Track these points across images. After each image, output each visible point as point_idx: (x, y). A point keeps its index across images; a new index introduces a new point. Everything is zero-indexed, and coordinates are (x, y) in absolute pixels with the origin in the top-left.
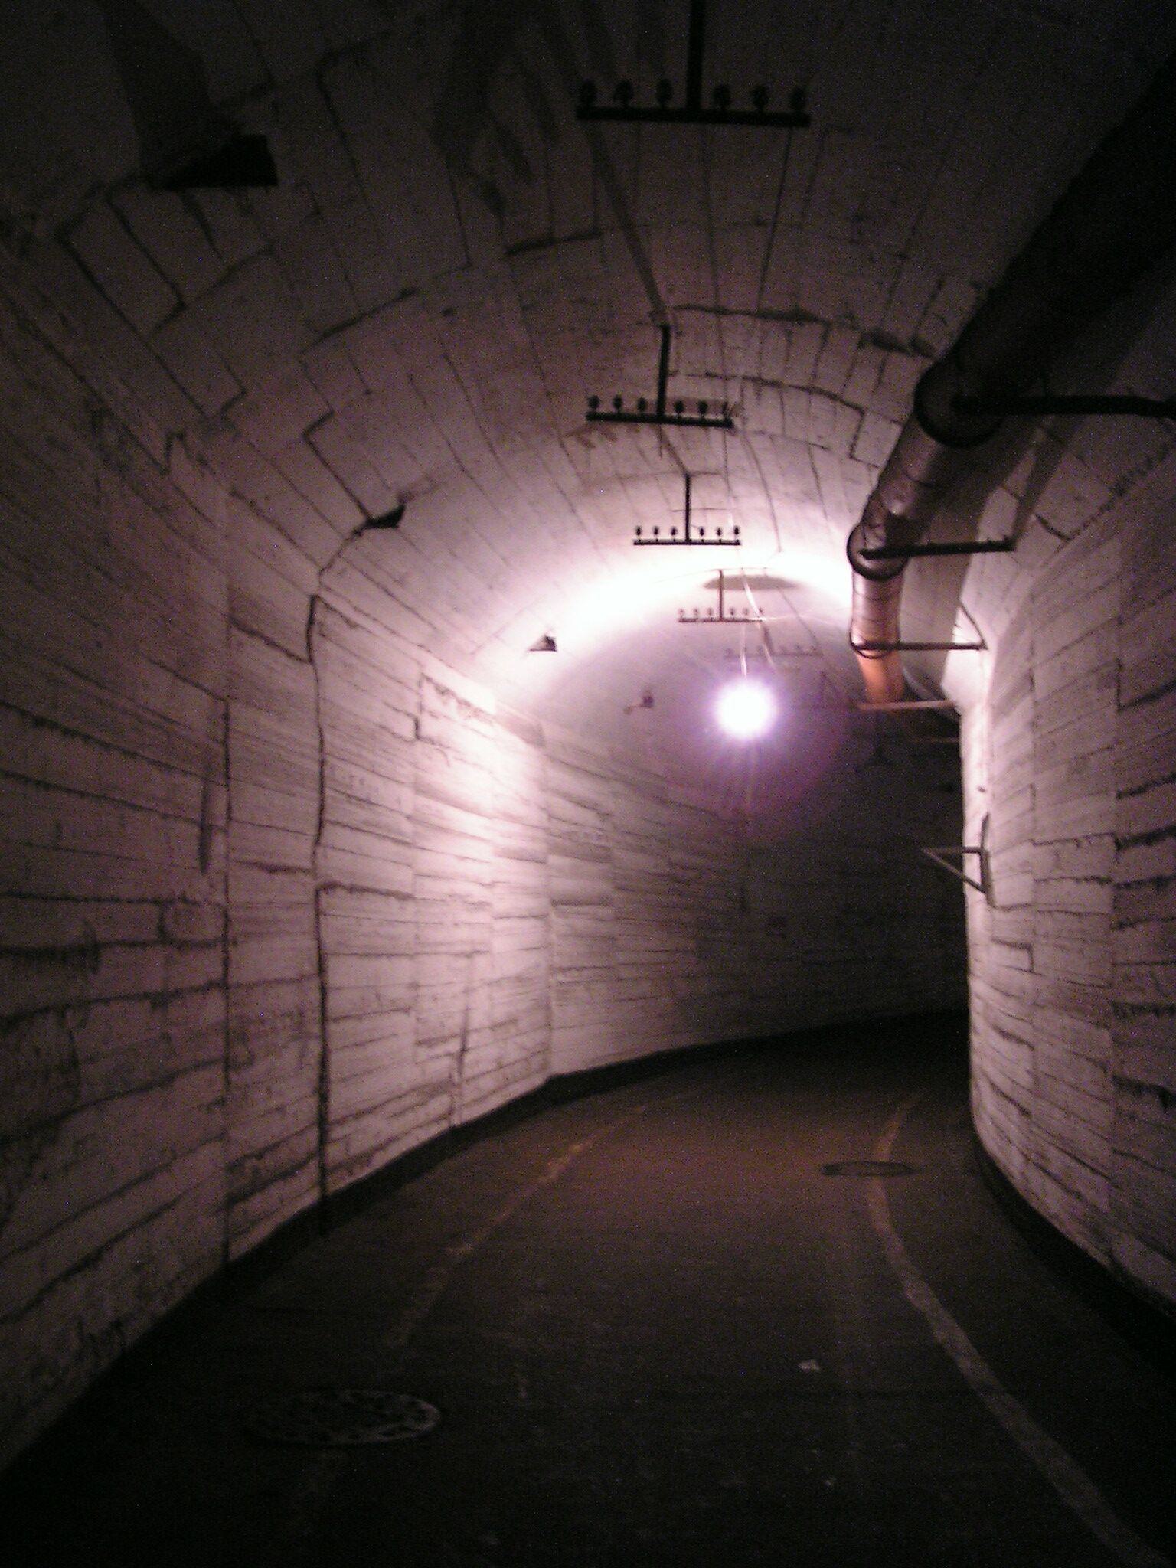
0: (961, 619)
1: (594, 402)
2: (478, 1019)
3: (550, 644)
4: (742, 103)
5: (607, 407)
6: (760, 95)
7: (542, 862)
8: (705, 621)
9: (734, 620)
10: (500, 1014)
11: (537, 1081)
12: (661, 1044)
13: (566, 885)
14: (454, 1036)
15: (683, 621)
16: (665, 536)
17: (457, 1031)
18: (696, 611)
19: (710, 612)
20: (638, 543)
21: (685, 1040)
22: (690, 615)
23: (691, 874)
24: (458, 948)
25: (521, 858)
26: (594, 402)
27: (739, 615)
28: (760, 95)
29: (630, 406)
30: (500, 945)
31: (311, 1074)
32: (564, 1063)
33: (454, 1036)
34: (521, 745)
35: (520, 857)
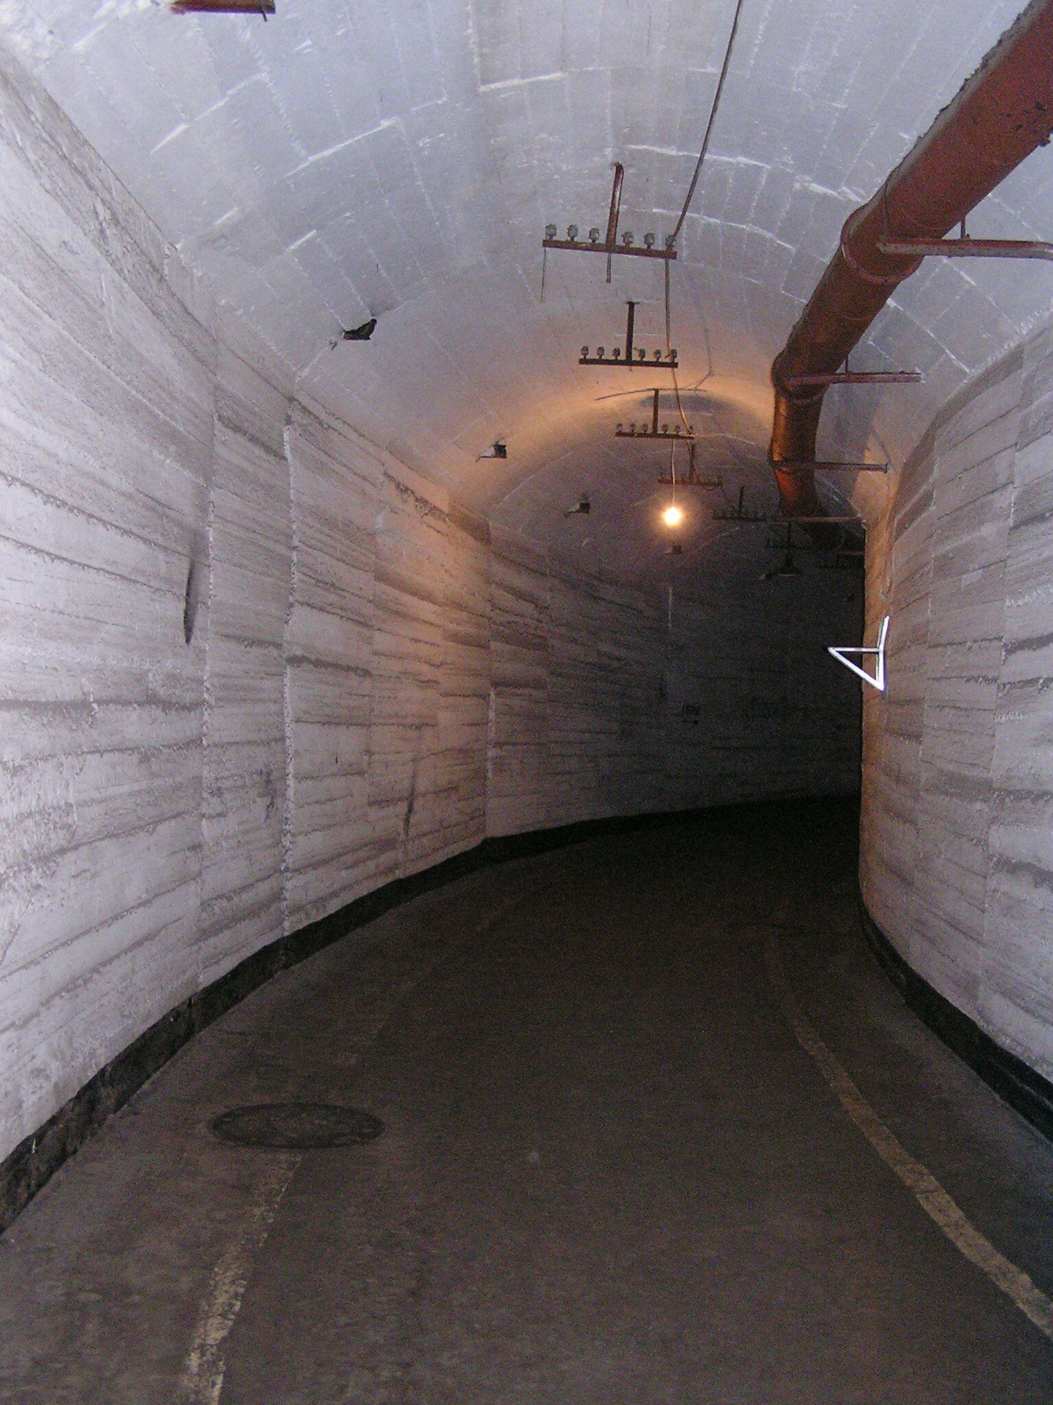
0: (871, 442)
1: (585, 350)
2: (423, 784)
3: (500, 451)
4: (638, 243)
5: (592, 355)
6: (649, 238)
7: (484, 647)
8: (640, 435)
9: (666, 436)
10: (442, 781)
11: (473, 843)
12: (584, 814)
13: (509, 669)
14: (400, 799)
15: (619, 434)
16: (608, 355)
17: (406, 795)
18: (633, 425)
19: (645, 426)
20: (584, 361)
21: (607, 811)
22: (627, 430)
23: (616, 664)
24: (409, 721)
25: (467, 643)
26: (585, 350)
27: (671, 432)
28: (649, 238)
29: (582, 237)
30: (444, 718)
31: (670, 339)
32: (499, 826)
33: (400, 799)
34: (471, 541)
35: (466, 641)
